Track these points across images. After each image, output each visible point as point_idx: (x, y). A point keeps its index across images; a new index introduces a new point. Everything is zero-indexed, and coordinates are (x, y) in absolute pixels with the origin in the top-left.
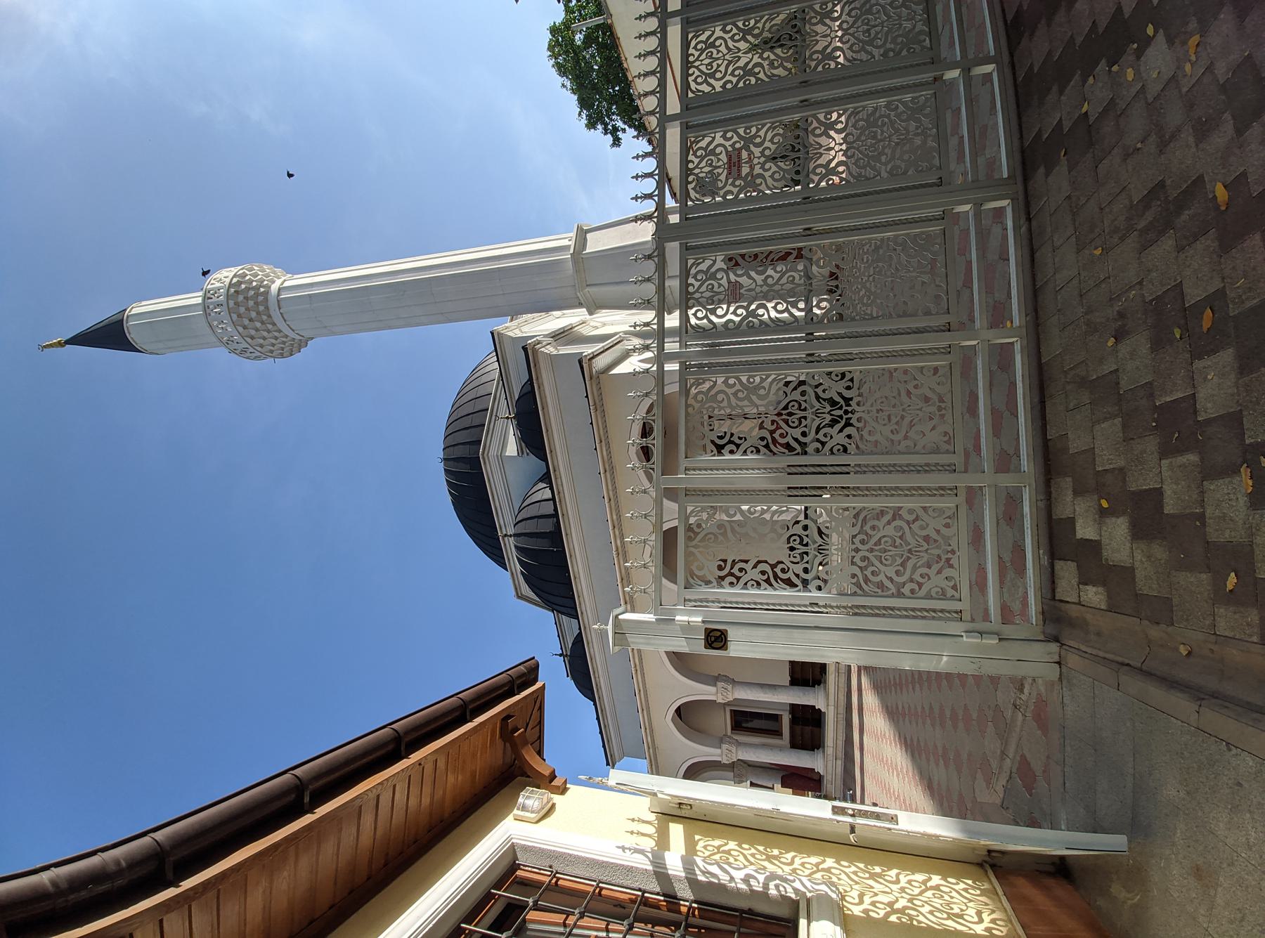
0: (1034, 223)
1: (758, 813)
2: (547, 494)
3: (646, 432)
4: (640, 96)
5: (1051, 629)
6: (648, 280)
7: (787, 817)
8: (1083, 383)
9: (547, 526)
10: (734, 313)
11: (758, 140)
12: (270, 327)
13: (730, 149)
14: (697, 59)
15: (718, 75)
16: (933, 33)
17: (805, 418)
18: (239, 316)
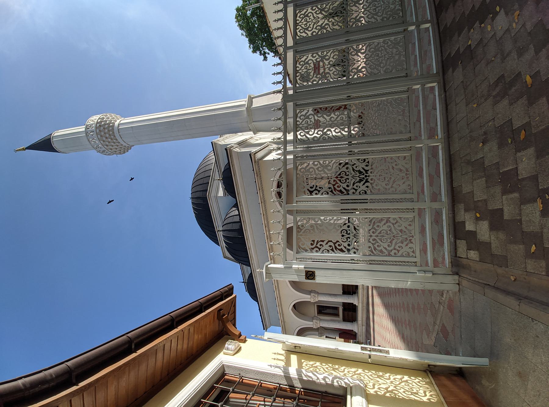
0: (447, 93)
1: (329, 350)
2: (237, 213)
3: (279, 185)
4: (275, 38)
5: (455, 270)
6: (280, 119)
7: (342, 352)
8: (468, 163)
9: (236, 227)
10: (317, 133)
11: (327, 57)
12: (115, 141)
13: (315, 61)
14: (300, 22)
15: (310, 29)
16: (403, 10)
17: (348, 179)
18: (101, 136)
